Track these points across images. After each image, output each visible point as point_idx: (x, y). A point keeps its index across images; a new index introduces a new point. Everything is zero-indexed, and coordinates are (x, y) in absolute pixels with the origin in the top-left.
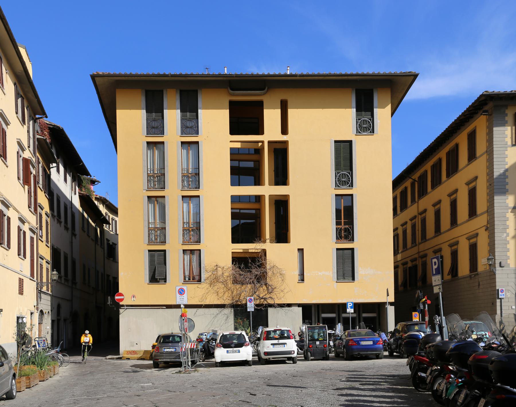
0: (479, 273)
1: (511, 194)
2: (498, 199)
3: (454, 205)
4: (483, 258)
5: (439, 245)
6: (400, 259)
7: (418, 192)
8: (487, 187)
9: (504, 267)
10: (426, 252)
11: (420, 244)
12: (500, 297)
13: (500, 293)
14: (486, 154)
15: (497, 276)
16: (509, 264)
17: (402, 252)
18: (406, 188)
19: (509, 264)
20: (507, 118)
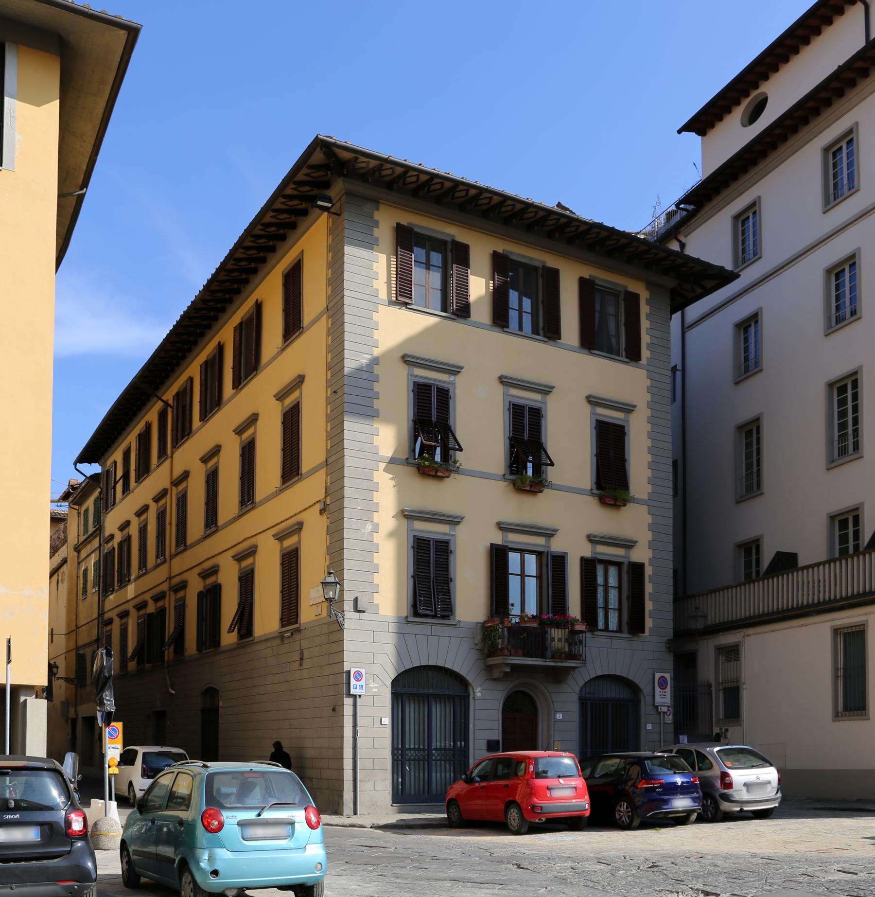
0: (302, 628)
1: (387, 421)
2: (353, 428)
3: (248, 452)
4: (312, 588)
5: (213, 557)
6: (133, 596)
7: (172, 431)
8: (327, 398)
9: (364, 612)
10: (185, 576)
11: (173, 556)
12: (352, 693)
13: (353, 682)
14: (325, 315)
15: (347, 635)
16: (378, 605)
17: (138, 577)
18: (148, 426)
19: (378, 605)
20: (376, 232)
